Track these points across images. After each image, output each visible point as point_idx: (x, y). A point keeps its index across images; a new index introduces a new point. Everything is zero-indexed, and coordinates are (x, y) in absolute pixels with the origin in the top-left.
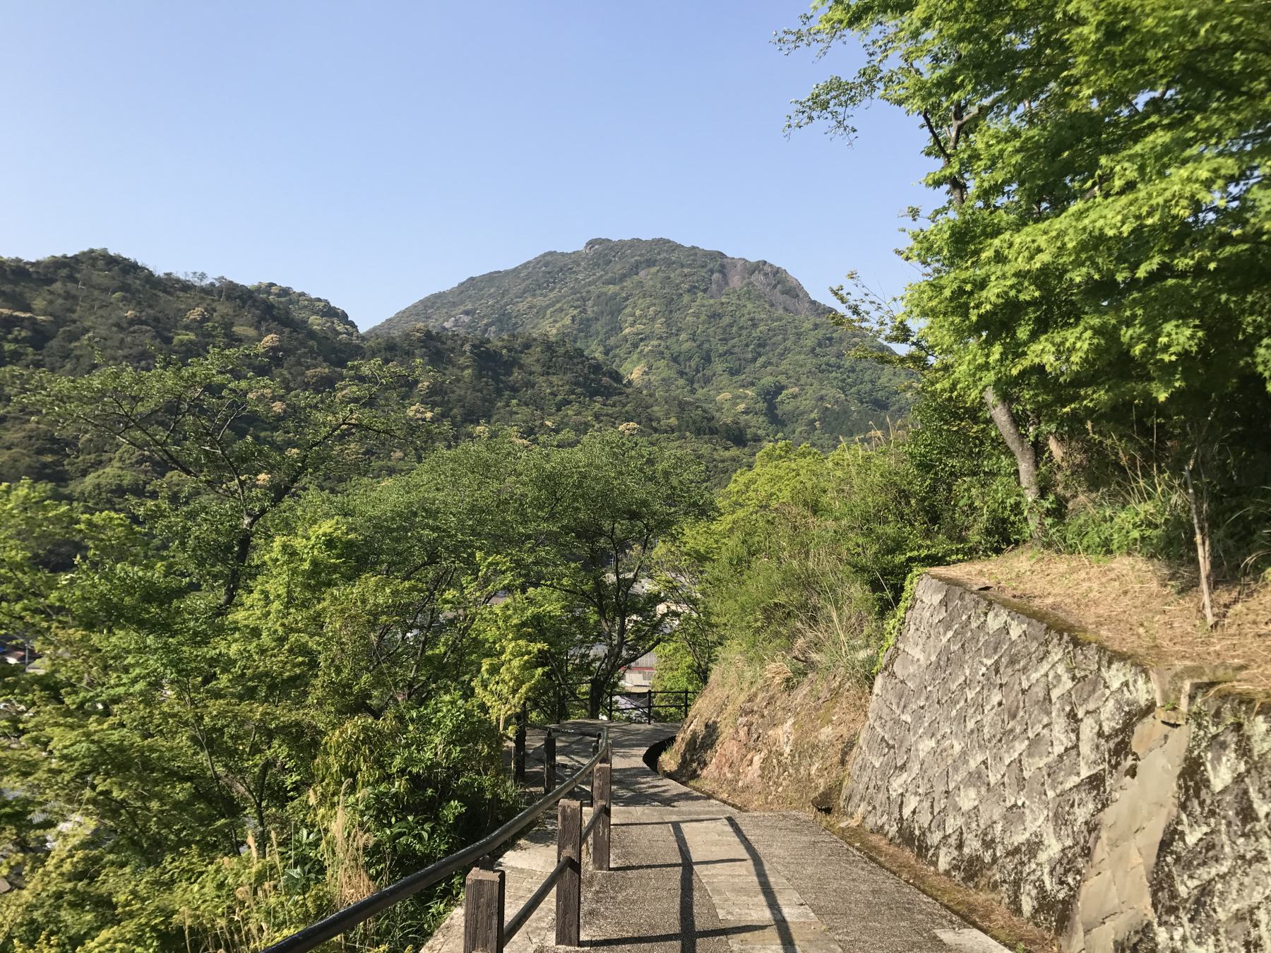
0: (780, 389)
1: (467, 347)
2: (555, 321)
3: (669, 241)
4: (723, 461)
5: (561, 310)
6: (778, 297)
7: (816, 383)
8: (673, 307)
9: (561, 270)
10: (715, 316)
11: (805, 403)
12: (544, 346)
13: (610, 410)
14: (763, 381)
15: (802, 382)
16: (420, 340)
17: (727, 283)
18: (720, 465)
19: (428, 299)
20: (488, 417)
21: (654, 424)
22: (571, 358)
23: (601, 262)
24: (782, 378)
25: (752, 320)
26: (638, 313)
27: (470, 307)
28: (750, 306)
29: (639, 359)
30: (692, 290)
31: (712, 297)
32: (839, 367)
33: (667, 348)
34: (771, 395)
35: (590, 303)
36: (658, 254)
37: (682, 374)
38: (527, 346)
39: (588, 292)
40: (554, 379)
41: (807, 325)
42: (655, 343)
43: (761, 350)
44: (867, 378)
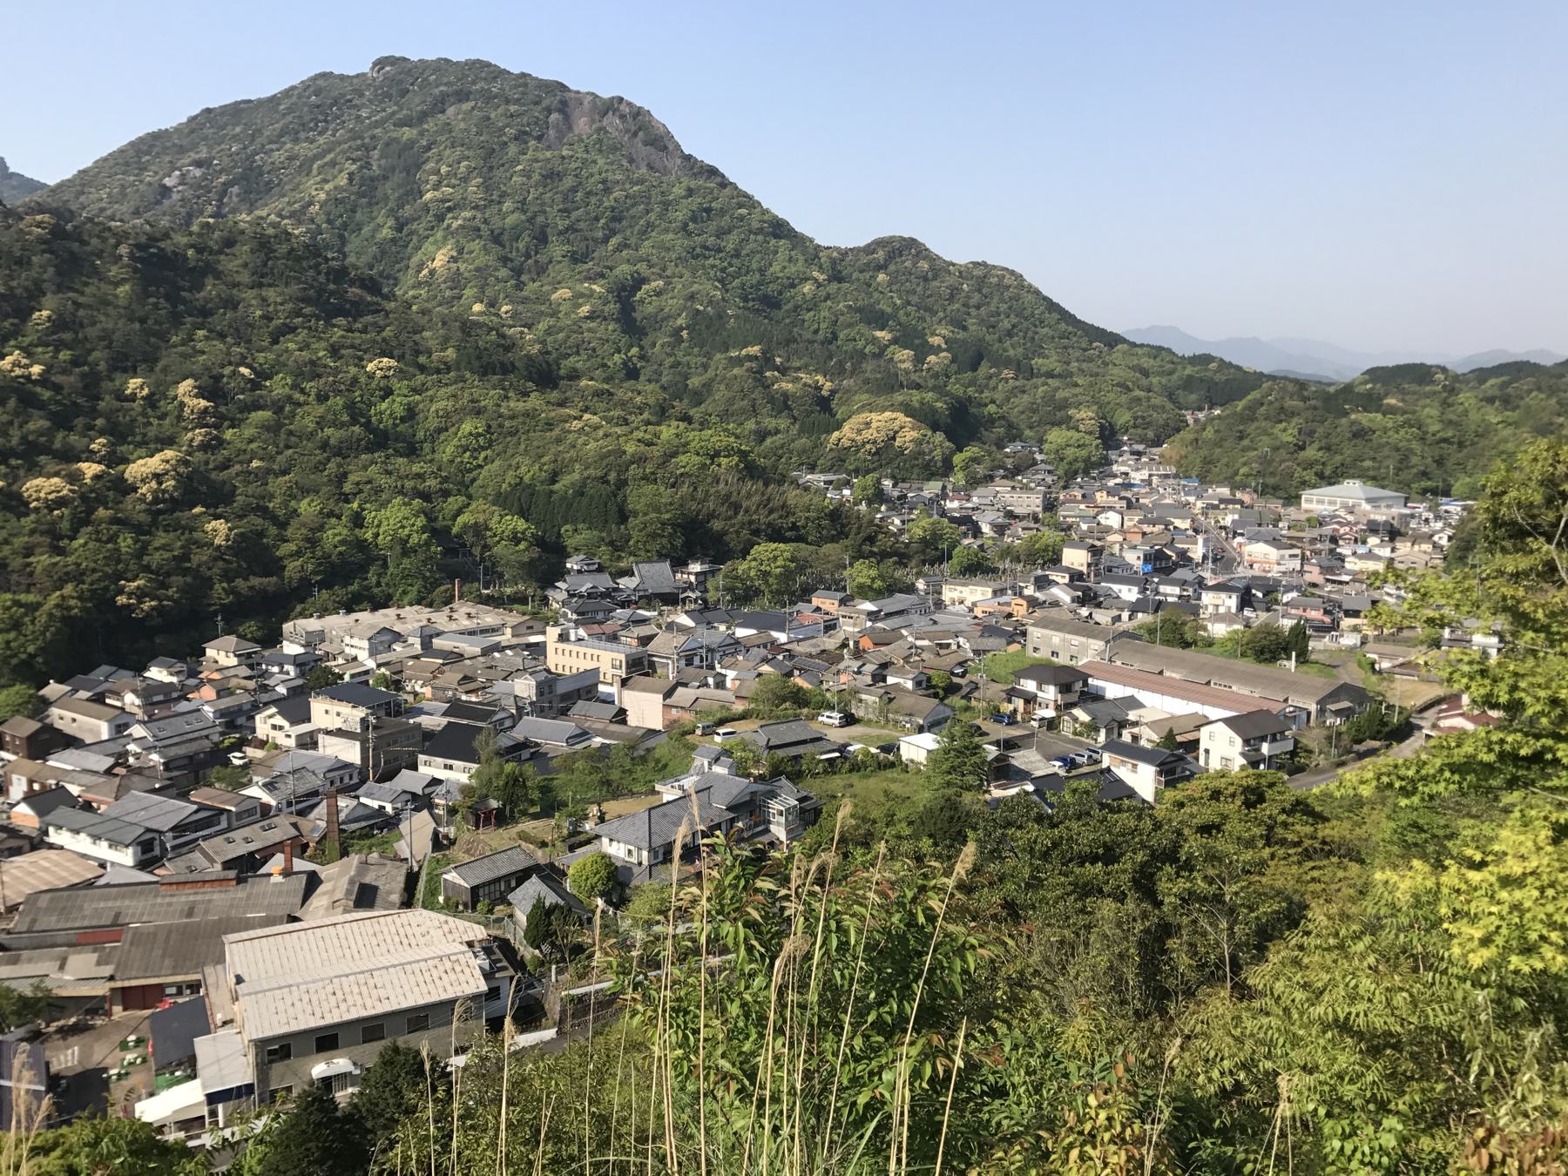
0: (639, 281)
1: (123, 250)
2: (326, 181)
3: (489, 65)
4: (512, 418)
5: (333, 164)
6: (640, 150)
7: (687, 274)
8: (494, 161)
9: (335, 103)
10: (552, 176)
11: (671, 303)
12: (255, 244)
13: (357, 338)
14: (617, 271)
15: (668, 273)
16: (41, 240)
17: (570, 128)
18: (507, 424)
19: (141, 140)
20: (150, 360)
21: (422, 359)
22: (298, 259)
23: (394, 91)
24: (642, 267)
25: (604, 182)
26: (444, 169)
27: (203, 154)
28: (601, 162)
29: (445, 238)
30: (521, 137)
31: (549, 148)
32: (719, 250)
33: (486, 222)
34: (625, 293)
35: (376, 154)
36: (473, 82)
37: (505, 260)
38: (229, 242)
39: (373, 137)
40: (270, 294)
41: (678, 191)
42: (467, 214)
43: (617, 225)
44: (754, 266)
